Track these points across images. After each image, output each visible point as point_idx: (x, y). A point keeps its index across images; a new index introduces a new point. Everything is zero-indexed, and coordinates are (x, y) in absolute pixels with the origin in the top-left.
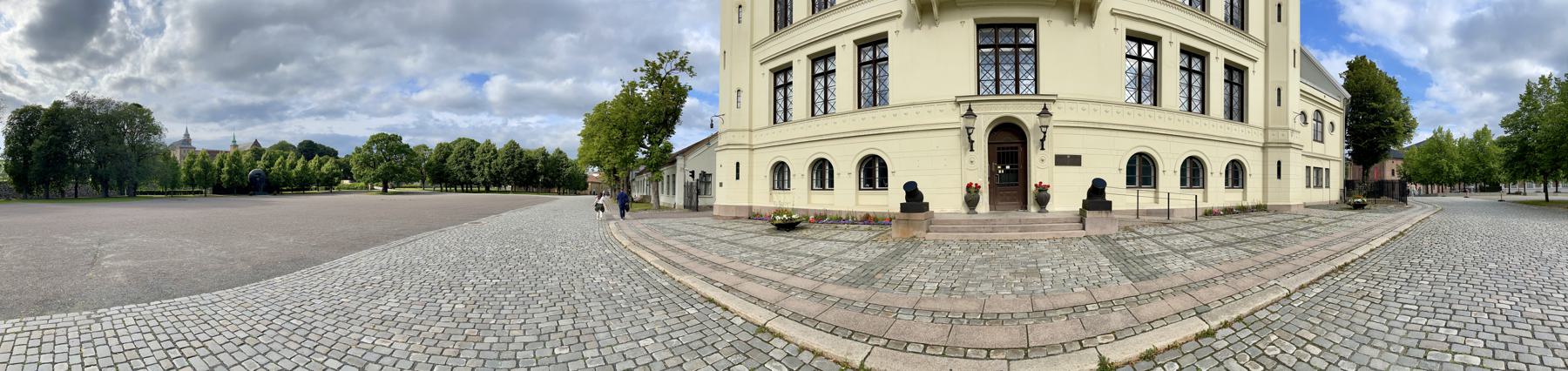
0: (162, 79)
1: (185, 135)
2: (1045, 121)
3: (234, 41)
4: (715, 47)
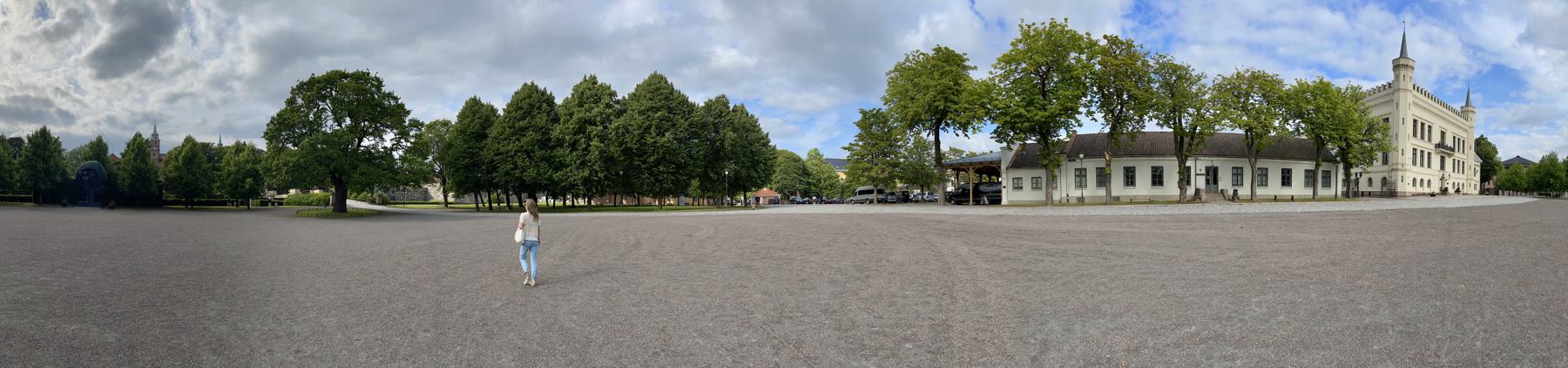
0: (216, 95)
1: (153, 135)
3: (286, 70)
4: (749, 61)
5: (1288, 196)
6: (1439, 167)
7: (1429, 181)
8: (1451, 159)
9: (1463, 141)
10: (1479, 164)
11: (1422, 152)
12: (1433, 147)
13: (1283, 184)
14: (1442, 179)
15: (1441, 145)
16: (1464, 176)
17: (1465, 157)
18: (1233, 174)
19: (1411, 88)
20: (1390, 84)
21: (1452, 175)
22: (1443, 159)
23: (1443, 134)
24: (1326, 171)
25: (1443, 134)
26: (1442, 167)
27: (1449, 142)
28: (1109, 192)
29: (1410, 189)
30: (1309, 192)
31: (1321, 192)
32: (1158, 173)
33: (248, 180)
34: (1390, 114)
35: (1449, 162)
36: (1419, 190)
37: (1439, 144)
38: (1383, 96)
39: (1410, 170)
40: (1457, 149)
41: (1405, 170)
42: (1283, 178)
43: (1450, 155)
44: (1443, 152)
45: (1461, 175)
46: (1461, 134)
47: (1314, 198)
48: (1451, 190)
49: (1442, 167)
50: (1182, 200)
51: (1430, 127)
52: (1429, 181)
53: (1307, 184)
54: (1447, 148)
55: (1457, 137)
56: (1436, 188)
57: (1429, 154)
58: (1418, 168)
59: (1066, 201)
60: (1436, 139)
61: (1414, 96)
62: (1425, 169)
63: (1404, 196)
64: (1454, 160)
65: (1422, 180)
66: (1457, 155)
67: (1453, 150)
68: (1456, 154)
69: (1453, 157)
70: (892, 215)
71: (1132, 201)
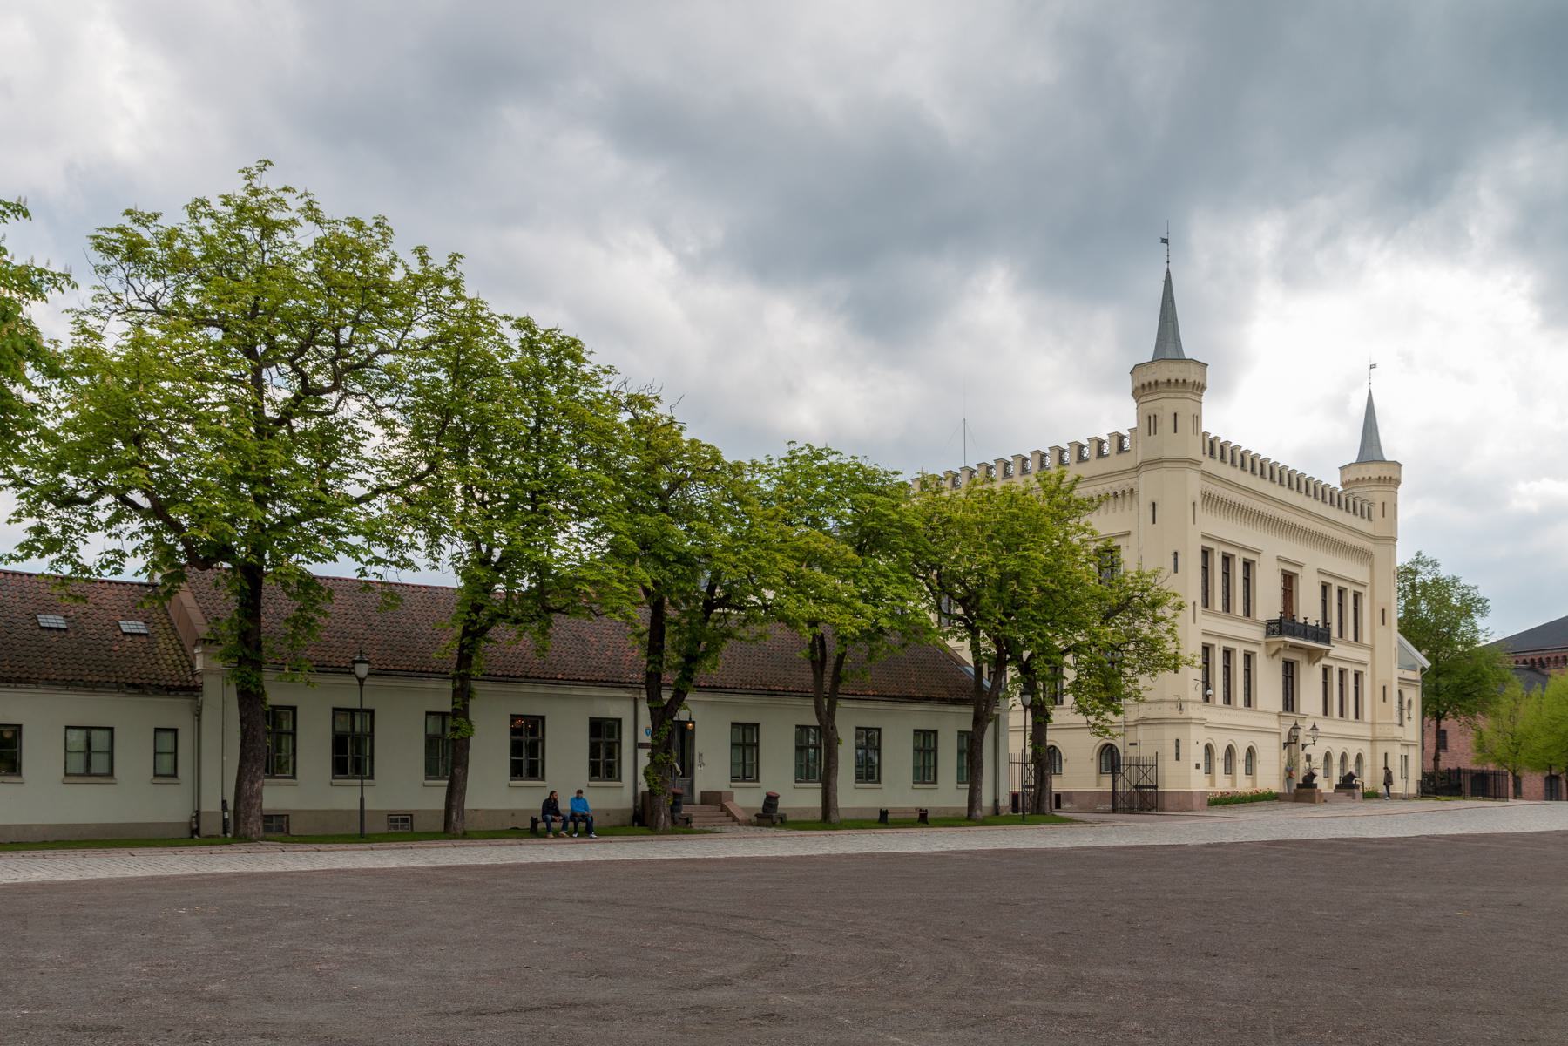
2: (1314, 732)
5: (905, 811)
6: (1277, 704)
7: (1251, 752)
8: (1317, 670)
9: (1357, 596)
10: (1415, 675)
11: (1228, 653)
12: (1257, 633)
13: (516, 771)
14: (1291, 742)
15: (1285, 625)
16: (1363, 730)
17: (1364, 655)
18: (733, 745)
19: (1196, 452)
20: (1121, 438)
21: (1325, 726)
22: (1289, 671)
23: (1289, 580)
24: (744, 726)
25: (1289, 580)
26: (1289, 702)
27: (1309, 609)
28: (455, 793)
29: (1198, 783)
30: (808, 798)
31: (851, 796)
32: (527, 738)
33: (242, 490)
34: (1128, 534)
35: (1309, 681)
36: (1223, 785)
37: (1280, 622)
38: (1112, 474)
39: (1201, 723)
40: (1335, 633)
41: (1187, 722)
42: (516, 748)
43: (1313, 656)
44: (1294, 647)
45: (1349, 727)
46: (1348, 569)
47: (969, 817)
48: (1324, 785)
49: (1289, 702)
50: (970, 817)
51: (1248, 565)
52: (1251, 752)
53: (804, 774)
54: (1306, 631)
55: (1335, 585)
56: (1269, 777)
57: (1248, 657)
58: (1217, 714)
59: (218, 830)
60: (1269, 605)
61: (1207, 475)
62: (1237, 716)
63: (1184, 803)
64: (1326, 670)
65: (1230, 751)
66: (1340, 651)
67: (1322, 634)
68: (1337, 649)
69: (1324, 661)
70: (24, 889)
71: (359, 832)
